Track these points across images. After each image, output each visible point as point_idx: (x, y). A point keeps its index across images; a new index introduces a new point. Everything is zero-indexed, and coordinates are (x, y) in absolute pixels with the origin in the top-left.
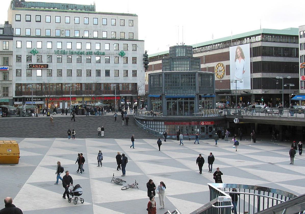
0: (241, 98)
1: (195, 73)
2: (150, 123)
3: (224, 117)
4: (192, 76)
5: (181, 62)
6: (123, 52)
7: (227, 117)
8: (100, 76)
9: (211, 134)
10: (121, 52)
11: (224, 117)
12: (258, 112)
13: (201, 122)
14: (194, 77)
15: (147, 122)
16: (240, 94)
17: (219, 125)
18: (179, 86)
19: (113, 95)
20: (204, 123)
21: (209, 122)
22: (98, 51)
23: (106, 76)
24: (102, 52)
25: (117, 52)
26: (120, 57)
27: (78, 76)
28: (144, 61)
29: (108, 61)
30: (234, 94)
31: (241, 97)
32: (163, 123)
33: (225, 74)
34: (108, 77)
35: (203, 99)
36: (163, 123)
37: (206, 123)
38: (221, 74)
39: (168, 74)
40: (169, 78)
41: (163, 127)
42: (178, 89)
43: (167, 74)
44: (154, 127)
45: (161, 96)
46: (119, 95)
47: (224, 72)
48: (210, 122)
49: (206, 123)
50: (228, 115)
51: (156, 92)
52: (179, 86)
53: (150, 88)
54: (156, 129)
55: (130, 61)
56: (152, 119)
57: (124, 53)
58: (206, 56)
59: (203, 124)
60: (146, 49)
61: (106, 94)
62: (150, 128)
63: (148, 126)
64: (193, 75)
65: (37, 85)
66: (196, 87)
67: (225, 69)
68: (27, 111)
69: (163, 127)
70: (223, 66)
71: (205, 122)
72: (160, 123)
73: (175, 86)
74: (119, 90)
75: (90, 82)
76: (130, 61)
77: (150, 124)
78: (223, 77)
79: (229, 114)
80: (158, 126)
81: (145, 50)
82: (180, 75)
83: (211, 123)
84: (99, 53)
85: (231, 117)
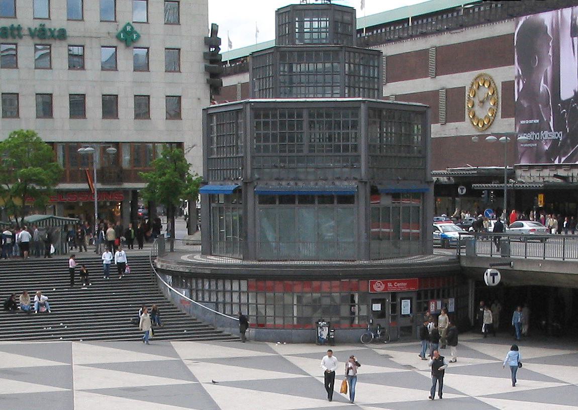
0: (541, 197)
1: (356, 105)
2: (200, 285)
3: (455, 263)
4: (266, 116)
5: (299, 66)
6: (132, 28)
7: (464, 263)
8: (18, 116)
9: (409, 324)
10: (124, 30)
11: (455, 263)
12: (266, 303)
13: (374, 283)
14: (264, 122)
15: (197, 284)
16: (541, 183)
17: (435, 292)
18: (302, 151)
19: (84, 186)
20: (383, 286)
21: (399, 282)
22: (44, 25)
23: (73, 118)
24: (55, 29)
25: (112, 29)
26: (121, 46)
27: (137, 116)
28: (208, 64)
29: (77, 62)
30: (523, 183)
31: (539, 196)
32: (244, 284)
33: (499, 114)
34: (79, 122)
35: (386, 201)
36: (244, 284)
37: (390, 285)
38: (483, 113)
39: (265, 109)
40: (266, 124)
41: (244, 299)
42: (298, 162)
43: (260, 109)
44: (214, 299)
45: (237, 191)
46: (118, 187)
47: (495, 108)
48: (404, 282)
49: (390, 285)
50: (467, 257)
51: (225, 171)
52: (302, 151)
53: (208, 159)
54: (221, 306)
55: (158, 61)
56: (208, 272)
57: (136, 32)
58: (439, 50)
59: (379, 290)
60: (213, 18)
61: (73, 180)
62: (203, 302)
63: (194, 297)
64: (262, 113)
65: (110, 147)
66: (359, 156)
67: (500, 95)
68: (410, 197)
69: (244, 299)
70: (492, 85)
71: (386, 283)
72: (235, 286)
73: (319, 151)
74: (122, 168)
75: (148, 139)
76: (158, 61)
77: (200, 288)
78: (491, 123)
79: (472, 257)
80: (228, 296)
81: (212, 20)
82: (305, 114)
83: (408, 286)
84: (49, 34)
85: (476, 265)
